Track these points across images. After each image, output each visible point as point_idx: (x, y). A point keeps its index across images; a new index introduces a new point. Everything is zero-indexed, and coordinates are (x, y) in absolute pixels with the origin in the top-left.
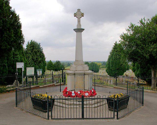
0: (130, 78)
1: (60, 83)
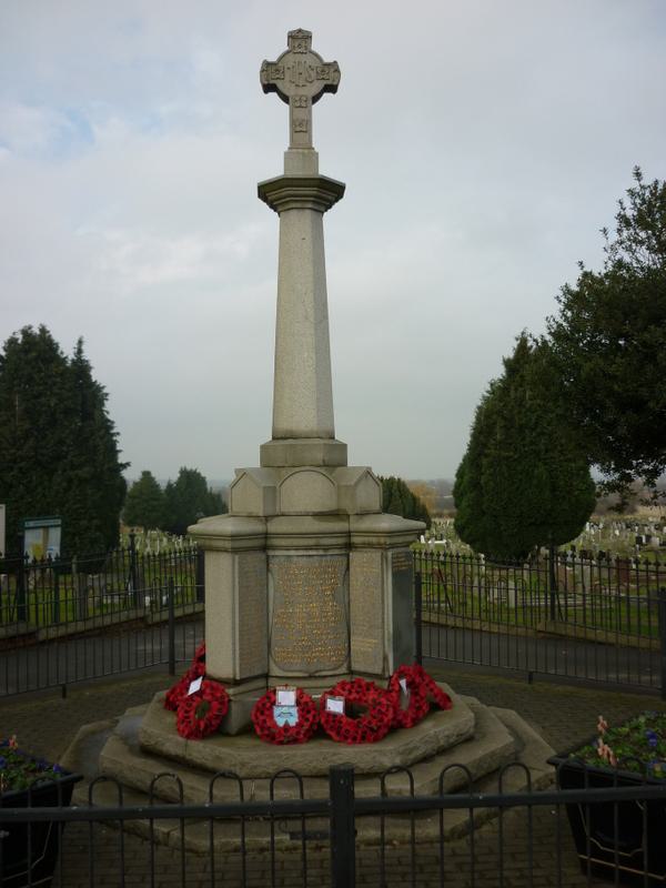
0: (468, 561)
1: (172, 613)
